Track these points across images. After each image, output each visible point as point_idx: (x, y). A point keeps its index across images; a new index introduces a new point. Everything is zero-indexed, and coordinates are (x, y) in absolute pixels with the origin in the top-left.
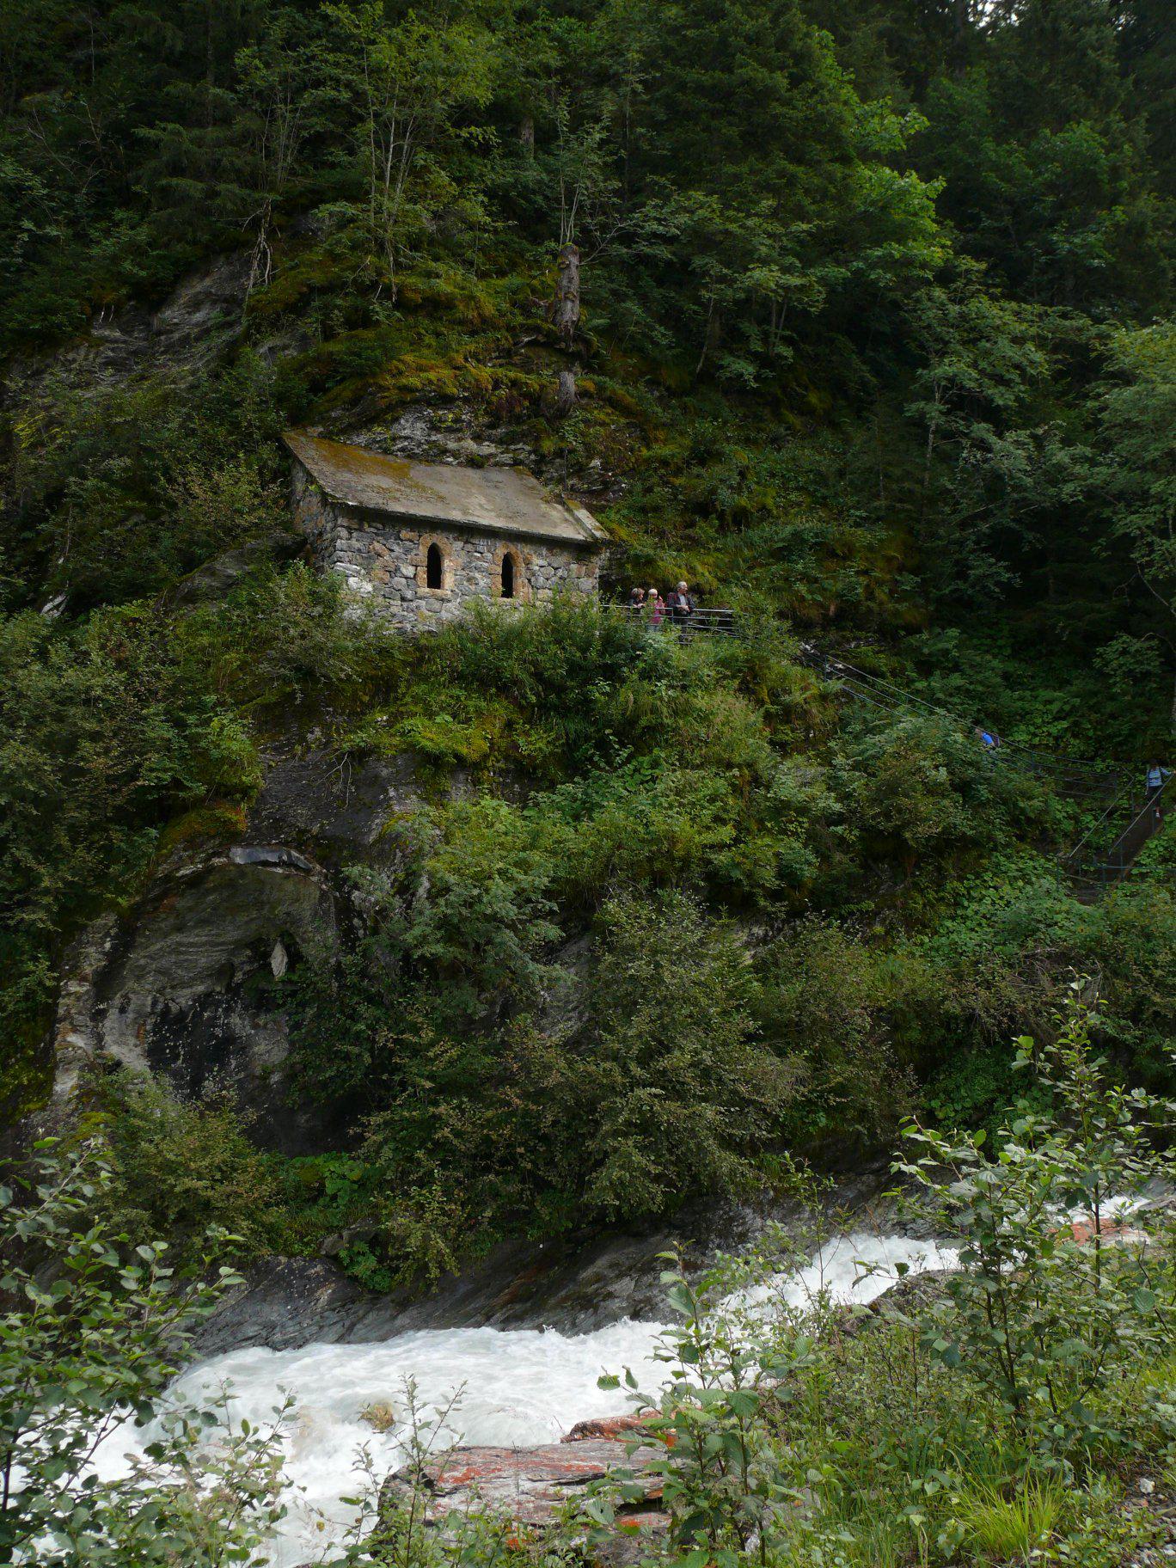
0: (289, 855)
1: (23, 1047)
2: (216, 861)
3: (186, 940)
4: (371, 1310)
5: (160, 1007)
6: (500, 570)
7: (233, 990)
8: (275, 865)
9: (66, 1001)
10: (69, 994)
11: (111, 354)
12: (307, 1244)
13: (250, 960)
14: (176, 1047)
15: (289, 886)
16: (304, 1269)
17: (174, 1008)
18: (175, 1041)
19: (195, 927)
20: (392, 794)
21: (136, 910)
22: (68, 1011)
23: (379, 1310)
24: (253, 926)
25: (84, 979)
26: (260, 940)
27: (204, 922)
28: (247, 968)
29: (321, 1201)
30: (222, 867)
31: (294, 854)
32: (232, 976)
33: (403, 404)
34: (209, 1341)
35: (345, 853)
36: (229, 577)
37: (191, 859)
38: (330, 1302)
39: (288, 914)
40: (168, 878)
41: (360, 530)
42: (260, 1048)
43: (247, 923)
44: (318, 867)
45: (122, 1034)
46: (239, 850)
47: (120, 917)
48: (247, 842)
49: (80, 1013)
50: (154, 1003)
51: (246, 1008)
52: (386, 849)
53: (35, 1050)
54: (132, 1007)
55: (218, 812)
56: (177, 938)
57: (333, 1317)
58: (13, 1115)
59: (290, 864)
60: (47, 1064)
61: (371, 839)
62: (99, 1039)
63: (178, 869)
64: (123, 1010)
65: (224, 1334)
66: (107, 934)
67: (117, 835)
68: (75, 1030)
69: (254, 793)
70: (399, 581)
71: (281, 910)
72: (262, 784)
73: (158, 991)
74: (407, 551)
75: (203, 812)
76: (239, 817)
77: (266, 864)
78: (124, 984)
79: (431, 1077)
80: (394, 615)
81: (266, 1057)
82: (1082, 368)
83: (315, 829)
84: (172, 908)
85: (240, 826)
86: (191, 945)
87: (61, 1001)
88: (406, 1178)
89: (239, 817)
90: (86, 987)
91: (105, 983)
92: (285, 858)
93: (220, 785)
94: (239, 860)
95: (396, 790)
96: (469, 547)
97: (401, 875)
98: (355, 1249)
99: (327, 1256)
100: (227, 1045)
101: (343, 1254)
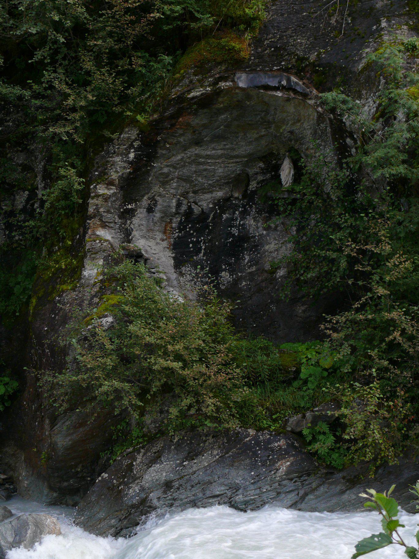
0: (289, 80)
1: (64, 238)
2: (223, 85)
3: (204, 153)
4: (324, 483)
5: (184, 208)
7: (249, 197)
8: (276, 89)
9: (95, 201)
10: (98, 196)
12: (275, 421)
13: (263, 172)
14: (198, 242)
15: (291, 108)
16: (269, 442)
17: (196, 210)
18: (198, 238)
19: (212, 141)
20: (384, 24)
21: (156, 127)
22: (97, 209)
23: (331, 484)
24: (263, 142)
25: (111, 183)
26: (271, 154)
27: (218, 138)
28: (260, 178)
29: (296, 384)
30: (230, 89)
31: (294, 79)
32: (248, 185)
34: (183, 495)
35: (338, 79)
37: (201, 83)
38: (288, 472)
39: (291, 132)
40: (181, 99)
42: (271, 246)
43: (257, 139)
44: (315, 92)
45: (150, 230)
46: (244, 76)
47: (142, 132)
48: (251, 69)
49: (108, 212)
50: (179, 205)
51: (259, 212)
52: (374, 77)
53: (72, 241)
54: (159, 207)
55: (223, 41)
57: (290, 485)
58: (52, 292)
59: (289, 88)
60: (78, 252)
61: (360, 66)
62: (127, 236)
63: (189, 91)
64: (150, 210)
65: (197, 490)
66: (131, 146)
67: (138, 62)
68: (104, 225)
69: (257, 24)
71: (285, 128)
72: (264, 15)
73: (182, 195)
75: (212, 40)
76: (242, 45)
77: (267, 88)
78: (151, 188)
79: (390, 285)
81: (274, 255)
83: (313, 57)
84: (188, 125)
85: (242, 54)
86: (208, 157)
87: (91, 201)
88: (358, 375)
89: (242, 45)
90: (113, 190)
91: (132, 187)
92: (284, 83)
93: (227, 16)
94: (241, 85)
95: (388, 21)
97: (385, 101)
98: (317, 429)
99: (292, 432)
100: (243, 242)
101: (305, 432)
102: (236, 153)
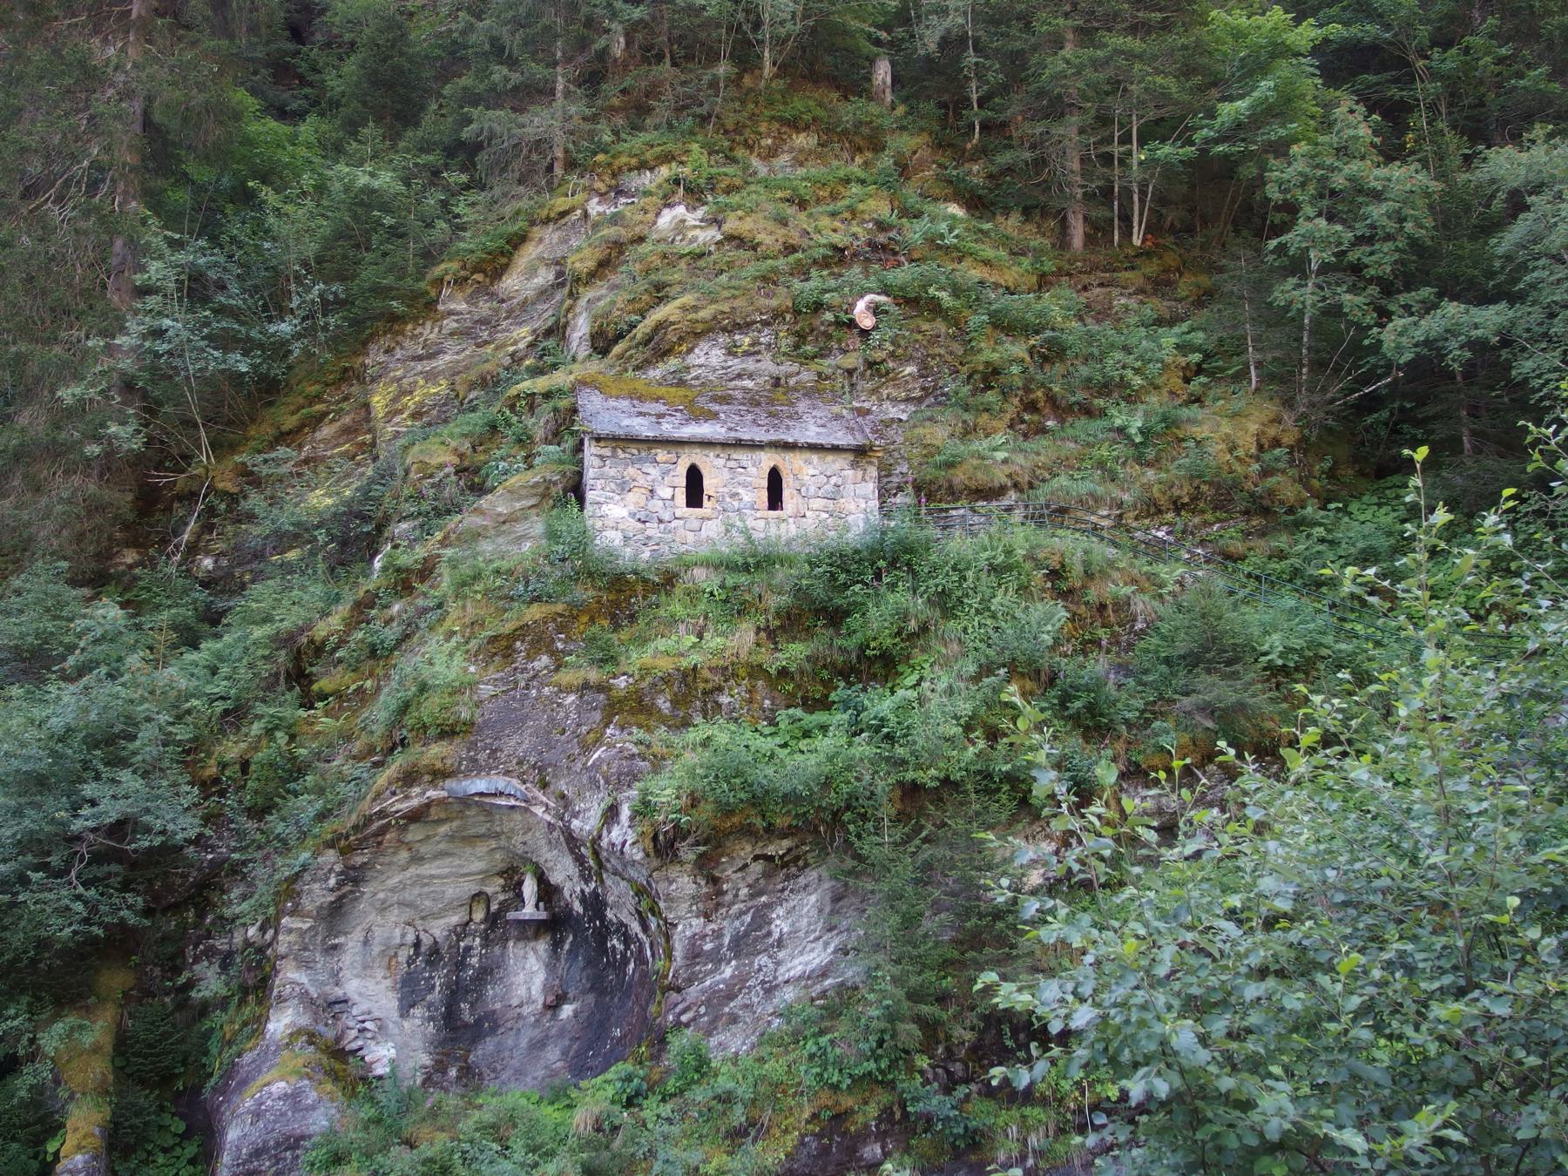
6: (765, 483)
11: (455, 325)
13: (504, 889)
17: (426, 941)
28: (501, 897)
33: (698, 336)
36: (500, 515)
41: (614, 456)
45: (366, 967)
56: (413, 871)
70: (656, 505)
74: (665, 473)
80: (649, 538)
82: (1473, 218)
86: (432, 877)
96: (732, 464)
102: (465, 871)
